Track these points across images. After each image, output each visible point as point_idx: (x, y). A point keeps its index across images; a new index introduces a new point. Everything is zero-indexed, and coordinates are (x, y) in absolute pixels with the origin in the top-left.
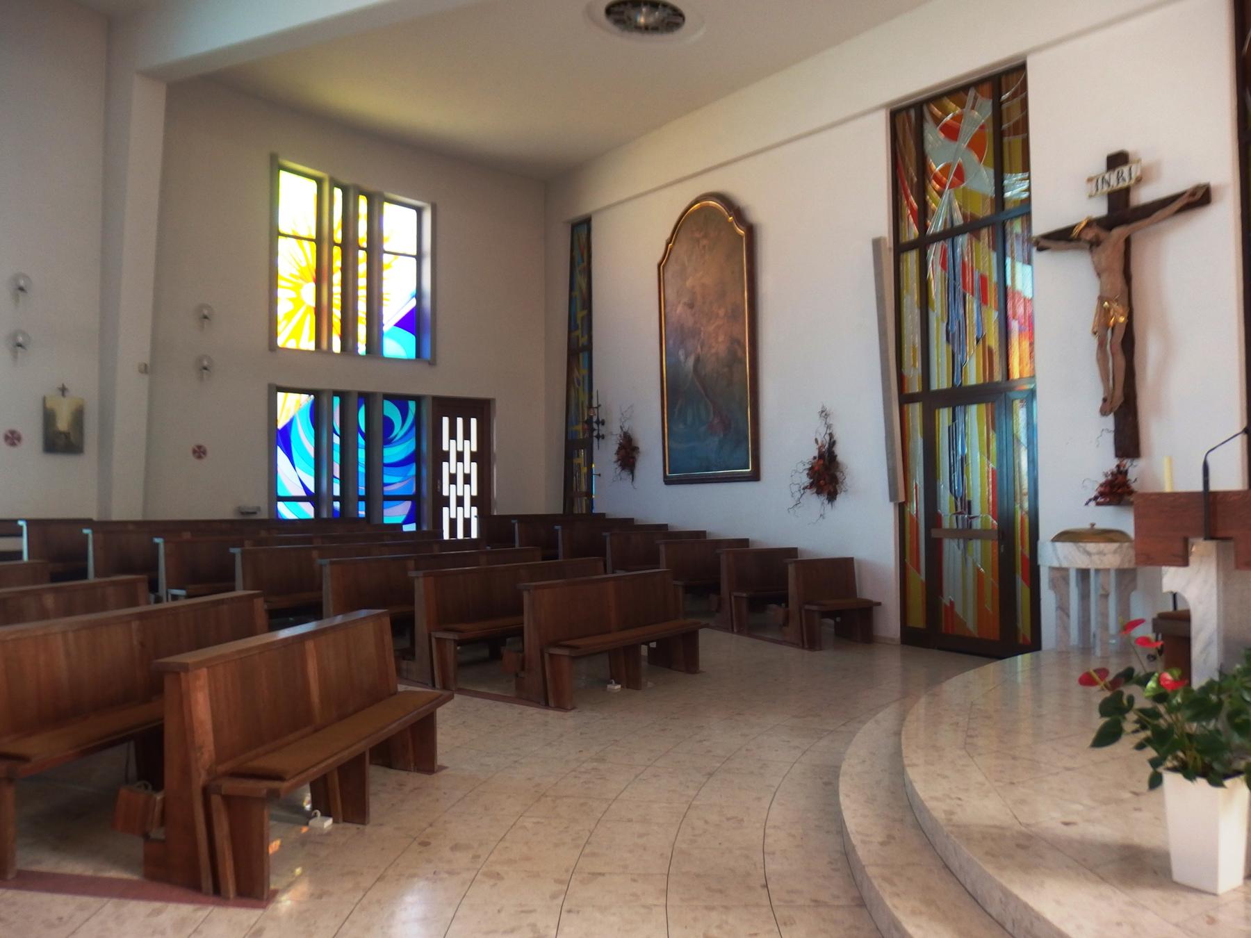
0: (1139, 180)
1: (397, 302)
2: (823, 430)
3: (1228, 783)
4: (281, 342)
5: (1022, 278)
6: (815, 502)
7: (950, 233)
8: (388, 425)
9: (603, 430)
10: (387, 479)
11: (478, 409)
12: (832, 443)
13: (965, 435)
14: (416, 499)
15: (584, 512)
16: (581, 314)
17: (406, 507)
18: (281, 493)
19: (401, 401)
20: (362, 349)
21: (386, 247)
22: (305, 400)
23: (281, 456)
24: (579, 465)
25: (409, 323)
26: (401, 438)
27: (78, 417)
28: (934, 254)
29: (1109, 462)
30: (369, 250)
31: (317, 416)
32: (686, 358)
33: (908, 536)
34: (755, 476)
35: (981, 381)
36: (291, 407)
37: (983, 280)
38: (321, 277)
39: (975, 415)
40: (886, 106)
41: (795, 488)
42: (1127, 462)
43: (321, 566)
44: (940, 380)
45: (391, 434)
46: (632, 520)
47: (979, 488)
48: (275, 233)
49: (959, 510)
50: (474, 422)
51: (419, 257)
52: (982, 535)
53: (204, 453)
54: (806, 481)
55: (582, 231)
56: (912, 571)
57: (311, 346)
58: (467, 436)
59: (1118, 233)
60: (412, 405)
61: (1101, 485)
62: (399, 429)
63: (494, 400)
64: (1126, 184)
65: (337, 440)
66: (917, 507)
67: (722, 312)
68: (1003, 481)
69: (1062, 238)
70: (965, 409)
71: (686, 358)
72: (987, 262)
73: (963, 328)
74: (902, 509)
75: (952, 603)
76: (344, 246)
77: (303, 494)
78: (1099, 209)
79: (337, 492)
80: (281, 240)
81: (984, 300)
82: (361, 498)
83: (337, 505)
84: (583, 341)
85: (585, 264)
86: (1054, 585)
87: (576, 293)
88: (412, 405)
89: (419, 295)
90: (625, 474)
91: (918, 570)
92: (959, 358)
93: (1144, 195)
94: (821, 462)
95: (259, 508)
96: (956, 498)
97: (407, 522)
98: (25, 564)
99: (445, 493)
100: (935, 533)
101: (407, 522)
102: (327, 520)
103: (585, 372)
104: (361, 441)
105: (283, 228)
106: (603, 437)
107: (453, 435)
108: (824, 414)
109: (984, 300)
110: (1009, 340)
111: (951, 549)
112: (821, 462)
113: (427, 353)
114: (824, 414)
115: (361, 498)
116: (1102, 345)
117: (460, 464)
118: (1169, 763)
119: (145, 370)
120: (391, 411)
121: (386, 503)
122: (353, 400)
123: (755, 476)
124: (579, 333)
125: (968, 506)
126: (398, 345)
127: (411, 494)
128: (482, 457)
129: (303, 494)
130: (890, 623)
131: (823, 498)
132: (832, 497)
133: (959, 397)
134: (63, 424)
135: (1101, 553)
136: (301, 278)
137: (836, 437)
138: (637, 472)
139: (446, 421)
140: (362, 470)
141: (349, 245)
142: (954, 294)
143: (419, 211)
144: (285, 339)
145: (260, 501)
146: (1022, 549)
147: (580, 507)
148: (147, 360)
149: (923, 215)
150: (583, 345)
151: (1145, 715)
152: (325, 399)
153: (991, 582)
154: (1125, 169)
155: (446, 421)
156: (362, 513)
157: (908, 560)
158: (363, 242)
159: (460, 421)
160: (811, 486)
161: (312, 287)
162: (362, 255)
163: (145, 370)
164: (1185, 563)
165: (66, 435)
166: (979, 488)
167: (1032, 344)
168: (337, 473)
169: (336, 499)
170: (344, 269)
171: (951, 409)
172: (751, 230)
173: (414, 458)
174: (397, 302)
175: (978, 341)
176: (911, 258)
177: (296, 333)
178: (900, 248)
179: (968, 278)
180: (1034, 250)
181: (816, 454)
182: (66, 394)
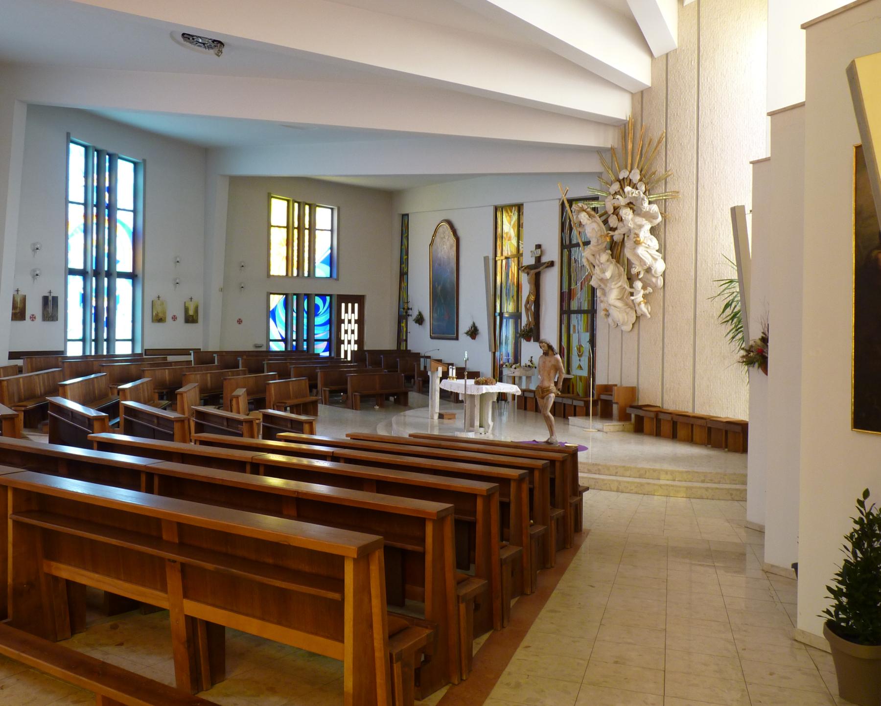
4: (272, 273)
8: (317, 308)
10: (316, 332)
11: (360, 300)
14: (329, 341)
15: (404, 349)
17: (325, 343)
18: (271, 338)
19: (323, 297)
20: (306, 274)
22: (281, 298)
23: (271, 321)
24: (403, 327)
27: (196, 310)
30: (309, 229)
31: (286, 304)
36: (276, 301)
38: (289, 243)
40: (494, 206)
43: (290, 368)
45: (318, 311)
48: (269, 226)
51: (332, 231)
55: (405, 217)
58: (353, 312)
60: (328, 298)
65: (295, 315)
76: (298, 228)
77: (280, 338)
79: (294, 338)
80: (272, 229)
82: (305, 340)
83: (294, 343)
85: (407, 234)
87: (403, 247)
88: (328, 298)
89: (332, 248)
95: (263, 345)
97: (325, 351)
98: (216, 365)
99: (342, 338)
101: (325, 351)
102: (291, 351)
103: (406, 284)
104: (305, 315)
105: (273, 224)
107: (346, 312)
113: (335, 276)
115: (305, 340)
117: (349, 325)
119: (221, 290)
120: (318, 301)
122: (302, 296)
124: (404, 265)
128: (360, 322)
134: (191, 312)
139: (343, 305)
140: (305, 328)
141: (300, 229)
143: (332, 209)
147: (403, 347)
148: (222, 287)
152: (290, 297)
156: (305, 347)
158: (307, 226)
159: (350, 305)
162: (307, 232)
163: (221, 290)
165: (192, 316)
168: (295, 329)
169: (294, 340)
170: (298, 239)
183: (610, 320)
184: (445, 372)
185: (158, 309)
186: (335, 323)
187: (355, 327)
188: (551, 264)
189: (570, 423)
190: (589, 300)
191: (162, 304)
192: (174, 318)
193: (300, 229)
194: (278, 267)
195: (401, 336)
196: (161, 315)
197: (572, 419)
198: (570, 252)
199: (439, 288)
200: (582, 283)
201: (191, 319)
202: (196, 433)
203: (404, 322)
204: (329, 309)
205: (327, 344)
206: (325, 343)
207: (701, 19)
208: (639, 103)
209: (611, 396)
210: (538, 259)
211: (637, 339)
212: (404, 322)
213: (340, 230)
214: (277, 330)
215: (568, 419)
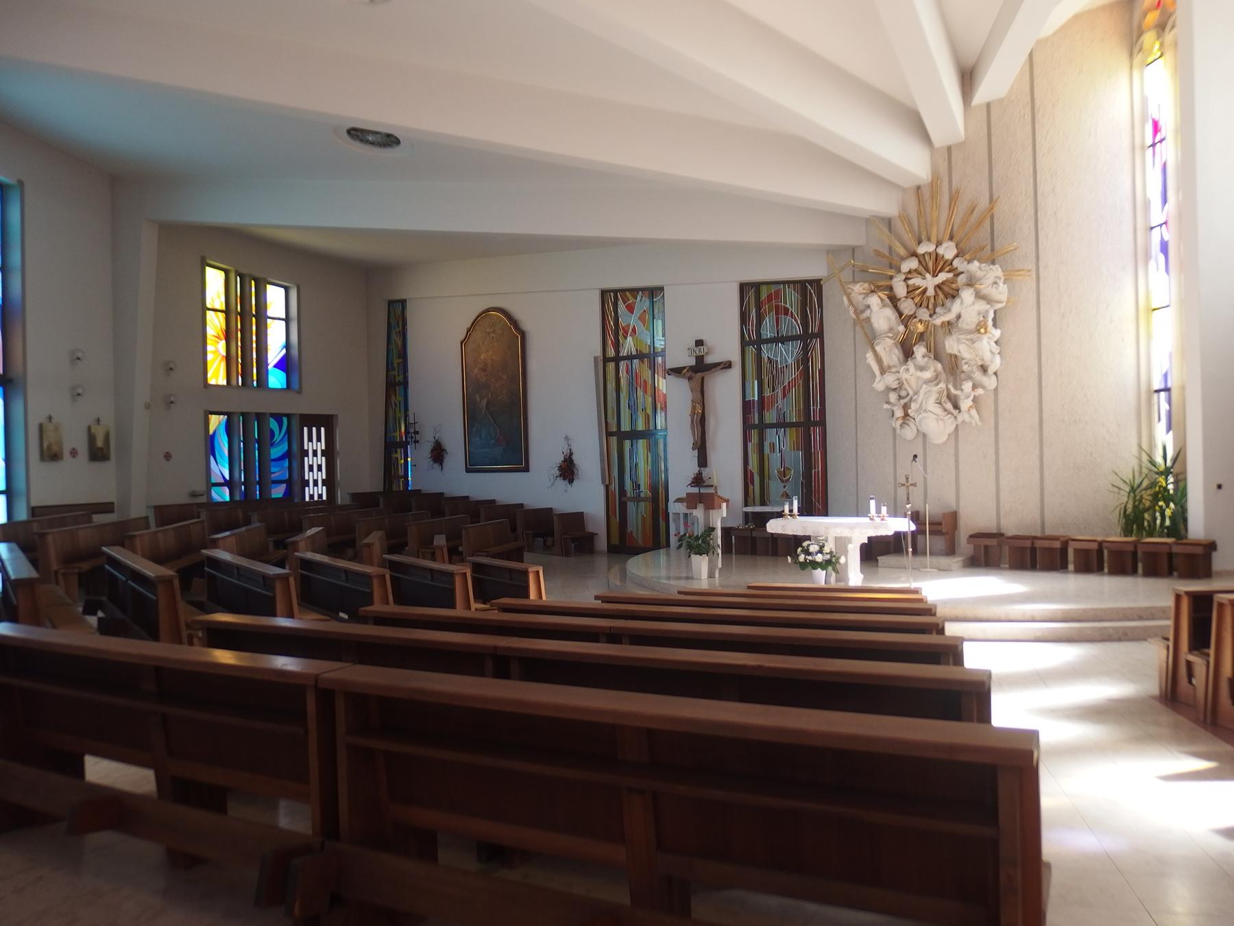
0: (707, 353)
1: (275, 352)
2: (566, 447)
3: (703, 555)
5: (662, 384)
6: (562, 484)
7: (630, 358)
9: (418, 437)
10: (273, 470)
11: (326, 422)
12: (571, 454)
13: (637, 453)
14: (289, 482)
15: (401, 489)
16: (396, 361)
17: (284, 486)
21: (269, 313)
25: (282, 365)
26: (278, 443)
28: (623, 365)
29: (696, 469)
32: (481, 400)
34: (526, 469)
35: (644, 429)
36: (216, 422)
37: (645, 382)
39: (642, 444)
41: (551, 477)
42: (702, 469)
44: (626, 427)
46: (443, 493)
47: (643, 480)
48: (204, 309)
50: (323, 429)
52: (644, 499)
53: (170, 457)
54: (558, 473)
56: (612, 517)
57: (225, 383)
58: (319, 440)
59: (699, 375)
60: (285, 420)
61: (693, 479)
62: (278, 433)
63: (337, 415)
64: (702, 354)
66: (615, 486)
67: (505, 377)
68: (654, 472)
69: (677, 371)
71: (481, 400)
72: (647, 374)
73: (636, 403)
74: (607, 487)
75: (632, 532)
77: (222, 481)
78: (692, 362)
81: (645, 392)
84: (400, 378)
86: (674, 520)
88: (285, 420)
90: (436, 466)
91: (616, 517)
92: (634, 416)
93: (710, 360)
94: (566, 464)
100: (624, 499)
106: (418, 442)
107: (310, 440)
108: (567, 439)
109: (645, 392)
111: (631, 507)
112: (566, 464)
113: (295, 385)
114: (567, 439)
116: (692, 422)
118: (692, 552)
120: (273, 424)
121: (273, 485)
123: (526, 469)
126: (276, 379)
127: (285, 479)
129: (222, 481)
130: (602, 543)
131: (567, 482)
132: (571, 481)
133: (634, 435)
134: (100, 443)
136: (218, 338)
137: (573, 451)
138: (444, 464)
139: (306, 429)
141: (244, 315)
144: (212, 380)
145: (201, 487)
146: (662, 506)
149: (617, 346)
150: (399, 381)
152: (235, 418)
153: (649, 521)
154: (702, 348)
155: (306, 429)
157: (610, 512)
159: (314, 429)
160: (561, 475)
161: (223, 343)
164: (696, 508)
165: (101, 449)
166: (643, 480)
167: (666, 415)
172: (523, 334)
173: (288, 455)
174: (275, 352)
175: (643, 410)
176: (611, 366)
177: (216, 376)
178: (606, 360)
179: (639, 381)
180: (667, 374)
181: (563, 459)
182: (100, 423)
183: (909, 433)
184: (552, 512)
185: (50, 437)
186: (296, 455)
187: (322, 461)
188: (728, 365)
189: (879, 565)
190: (799, 410)
191: (57, 429)
192: (74, 453)
193: (244, 315)
194: (217, 375)
195: (390, 470)
196: (55, 448)
197: (881, 559)
198: (759, 350)
199: (484, 402)
200: (784, 388)
201: (98, 454)
202: (453, 606)
203: (399, 452)
204: (287, 436)
205: (287, 486)
206: (284, 486)
207: (1035, 68)
208: (944, 160)
209: (940, 526)
210: (700, 359)
211: (953, 452)
212: (399, 452)
213: (296, 319)
214: (221, 469)
215: (877, 561)
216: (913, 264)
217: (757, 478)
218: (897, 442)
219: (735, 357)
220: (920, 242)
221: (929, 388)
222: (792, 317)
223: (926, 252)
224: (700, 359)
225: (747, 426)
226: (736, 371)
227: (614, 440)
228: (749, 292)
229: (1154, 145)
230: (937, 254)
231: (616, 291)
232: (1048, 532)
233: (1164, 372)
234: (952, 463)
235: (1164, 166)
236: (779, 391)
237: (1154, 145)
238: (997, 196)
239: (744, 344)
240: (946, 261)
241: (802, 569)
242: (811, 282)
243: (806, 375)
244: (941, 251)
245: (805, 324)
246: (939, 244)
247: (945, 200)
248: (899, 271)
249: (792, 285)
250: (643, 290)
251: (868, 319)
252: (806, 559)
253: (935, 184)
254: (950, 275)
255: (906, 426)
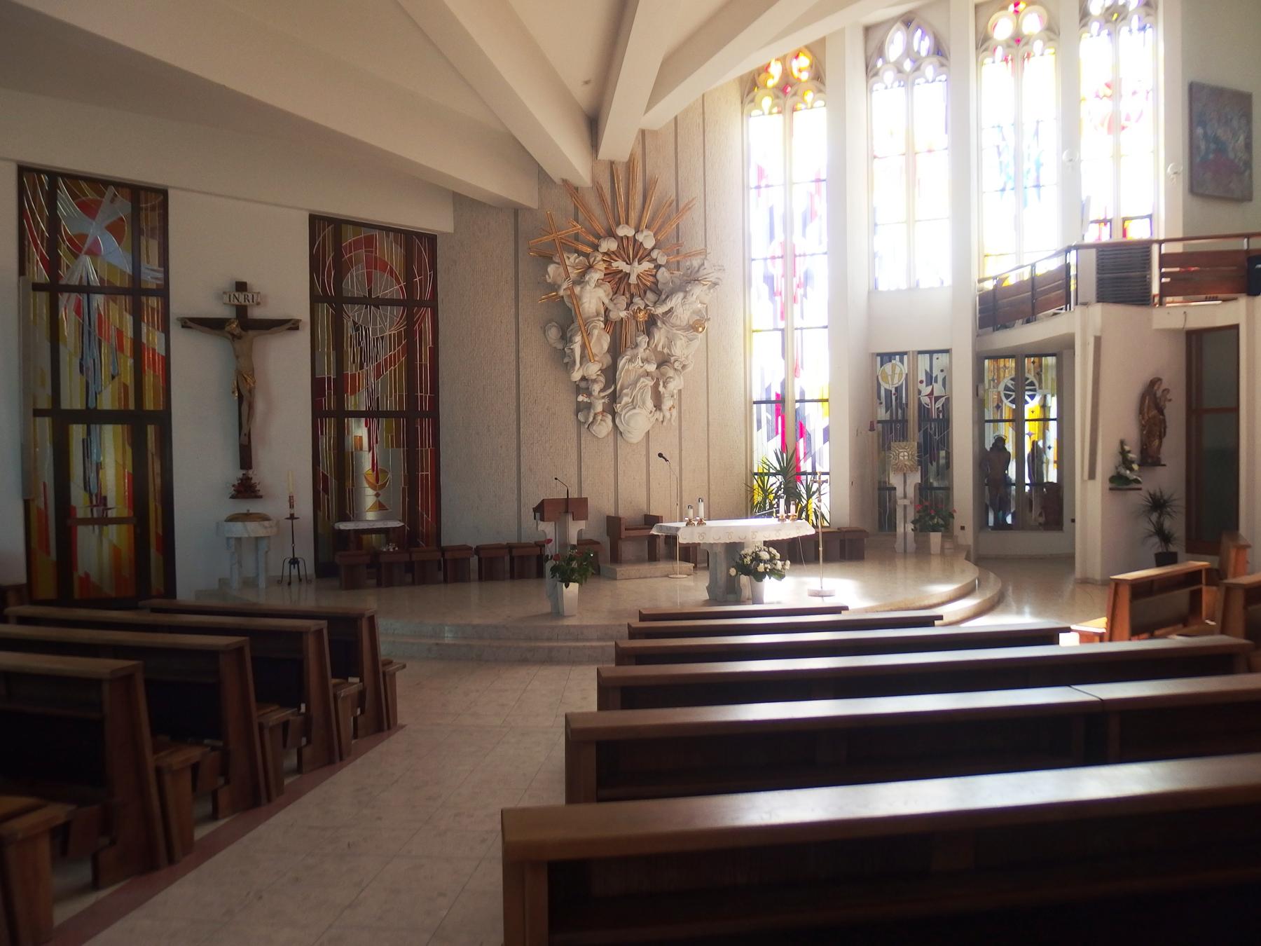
33: (34, 524)
37: (120, 334)
49: (94, 503)
52: (118, 521)
70: (100, 429)
91: (48, 553)
92: (92, 388)
93: (256, 313)
96: (91, 495)
110: (977, 433)
125: (104, 500)
135: (369, 458)
142: (84, 332)
151: (636, 257)
171: (85, 426)
210: (241, 310)
216: (612, 245)
217: (333, 483)
218: (583, 439)
219: (303, 313)
220: (618, 224)
221: (647, 382)
222: (392, 275)
223: (625, 236)
224: (241, 310)
225: (318, 413)
226: (304, 335)
227: (45, 424)
228: (324, 230)
229: (758, 187)
230: (635, 240)
231: (54, 175)
232: (524, 540)
233: (766, 385)
234: (644, 463)
235: (771, 211)
236: (370, 368)
237: (758, 187)
238: (670, 194)
239: (315, 299)
240: (645, 249)
241: (758, 581)
242: (421, 236)
243: (410, 351)
244: (640, 238)
245: (410, 286)
246: (637, 231)
247: (639, 186)
248: (596, 248)
249: (391, 234)
250: (120, 185)
251: (579, 298)
252: (766, 569)
253: (630, 166)
254: (652, 266)
255: (604, 424)
